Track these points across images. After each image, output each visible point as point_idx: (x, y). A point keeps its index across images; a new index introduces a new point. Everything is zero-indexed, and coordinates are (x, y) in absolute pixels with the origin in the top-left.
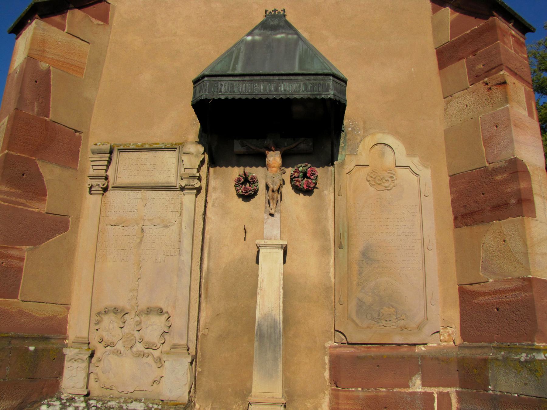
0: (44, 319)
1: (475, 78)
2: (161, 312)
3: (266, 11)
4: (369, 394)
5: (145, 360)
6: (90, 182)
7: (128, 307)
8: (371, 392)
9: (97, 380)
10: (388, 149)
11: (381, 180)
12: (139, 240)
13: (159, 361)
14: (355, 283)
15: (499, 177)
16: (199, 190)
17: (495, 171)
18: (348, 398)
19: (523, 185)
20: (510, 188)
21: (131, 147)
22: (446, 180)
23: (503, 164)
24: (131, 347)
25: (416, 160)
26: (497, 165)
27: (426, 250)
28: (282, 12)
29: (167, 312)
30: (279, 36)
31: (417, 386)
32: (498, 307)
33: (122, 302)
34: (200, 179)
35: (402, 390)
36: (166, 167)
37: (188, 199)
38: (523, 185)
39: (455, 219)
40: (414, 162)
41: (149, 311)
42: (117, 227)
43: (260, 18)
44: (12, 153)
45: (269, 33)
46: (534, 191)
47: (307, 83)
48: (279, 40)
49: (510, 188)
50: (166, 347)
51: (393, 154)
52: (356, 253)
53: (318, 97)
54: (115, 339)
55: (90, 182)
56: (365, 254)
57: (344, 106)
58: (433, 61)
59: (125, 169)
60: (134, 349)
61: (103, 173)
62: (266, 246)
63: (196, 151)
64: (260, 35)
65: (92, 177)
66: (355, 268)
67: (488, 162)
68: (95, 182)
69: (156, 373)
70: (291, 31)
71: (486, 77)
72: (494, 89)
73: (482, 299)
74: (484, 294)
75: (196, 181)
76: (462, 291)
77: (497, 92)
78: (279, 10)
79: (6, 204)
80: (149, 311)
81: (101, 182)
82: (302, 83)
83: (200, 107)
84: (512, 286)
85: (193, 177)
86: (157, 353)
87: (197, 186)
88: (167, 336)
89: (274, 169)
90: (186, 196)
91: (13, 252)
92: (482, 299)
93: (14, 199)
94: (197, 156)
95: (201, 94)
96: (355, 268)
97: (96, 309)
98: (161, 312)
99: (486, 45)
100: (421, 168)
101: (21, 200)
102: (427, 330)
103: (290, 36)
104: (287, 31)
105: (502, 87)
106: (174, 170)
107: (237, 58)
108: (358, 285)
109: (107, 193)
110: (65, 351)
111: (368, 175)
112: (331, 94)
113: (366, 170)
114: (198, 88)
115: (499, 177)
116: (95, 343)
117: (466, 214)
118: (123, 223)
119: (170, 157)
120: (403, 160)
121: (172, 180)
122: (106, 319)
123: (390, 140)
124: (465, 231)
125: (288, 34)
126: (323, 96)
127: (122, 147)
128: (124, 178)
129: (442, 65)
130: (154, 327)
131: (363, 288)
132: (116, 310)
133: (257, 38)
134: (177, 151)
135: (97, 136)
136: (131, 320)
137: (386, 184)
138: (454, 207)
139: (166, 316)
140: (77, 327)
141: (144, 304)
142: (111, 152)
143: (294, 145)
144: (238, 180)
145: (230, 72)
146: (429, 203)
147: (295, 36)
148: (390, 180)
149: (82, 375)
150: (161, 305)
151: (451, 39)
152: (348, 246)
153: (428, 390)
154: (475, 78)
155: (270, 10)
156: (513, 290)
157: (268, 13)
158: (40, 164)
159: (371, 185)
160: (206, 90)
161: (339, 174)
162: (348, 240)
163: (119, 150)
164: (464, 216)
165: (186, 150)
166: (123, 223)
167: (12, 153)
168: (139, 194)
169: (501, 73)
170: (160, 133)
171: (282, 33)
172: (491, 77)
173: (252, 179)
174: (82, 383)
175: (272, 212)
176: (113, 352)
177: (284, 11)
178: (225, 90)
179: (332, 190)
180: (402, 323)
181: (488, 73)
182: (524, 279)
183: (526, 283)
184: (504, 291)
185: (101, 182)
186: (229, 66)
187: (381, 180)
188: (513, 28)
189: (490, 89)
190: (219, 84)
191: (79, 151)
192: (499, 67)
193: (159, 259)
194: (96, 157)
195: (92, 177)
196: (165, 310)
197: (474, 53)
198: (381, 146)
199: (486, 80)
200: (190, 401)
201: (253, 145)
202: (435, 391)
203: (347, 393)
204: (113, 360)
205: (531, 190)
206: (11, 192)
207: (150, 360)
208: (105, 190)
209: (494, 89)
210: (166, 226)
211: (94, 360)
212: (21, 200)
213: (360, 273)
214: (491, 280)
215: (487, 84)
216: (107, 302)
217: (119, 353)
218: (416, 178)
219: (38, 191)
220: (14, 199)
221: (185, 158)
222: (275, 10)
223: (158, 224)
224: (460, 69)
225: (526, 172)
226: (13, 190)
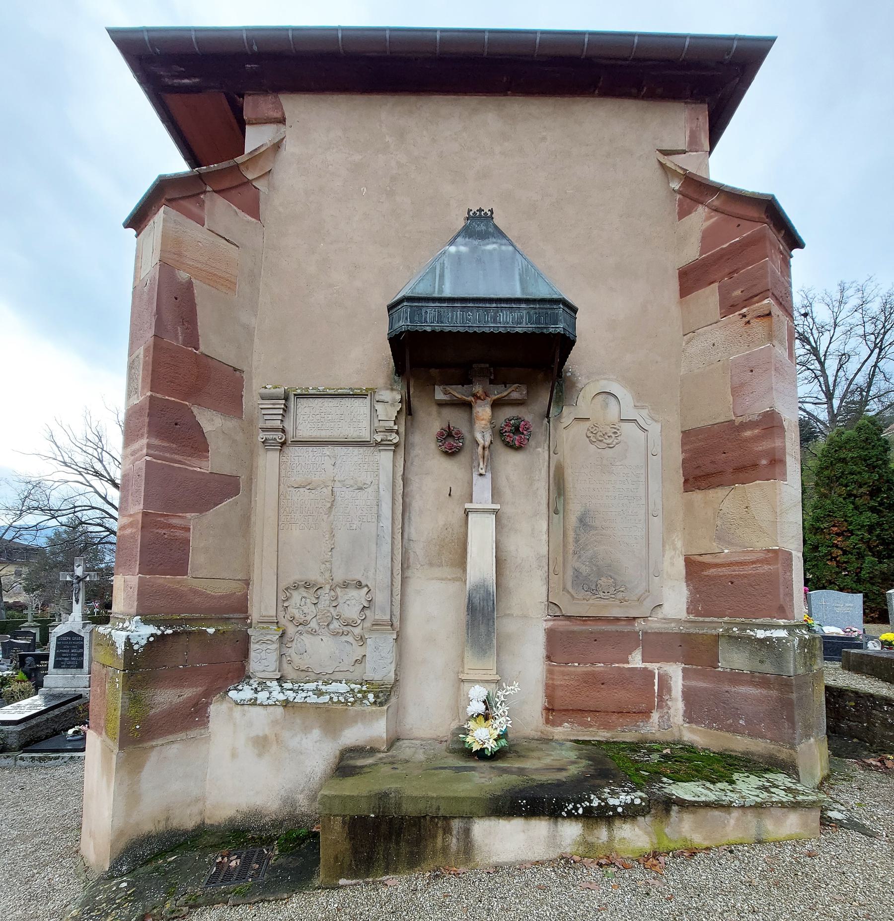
0: (221, 597)
1: (729, 307)
2: (359, 585)
3: (470, 211)
4: (585, 670)
5: (344, 638)
6: (262, 436)
7: (321, 580)
8: (588, 668)
9: (290, 662)
10: (612, 399)
11: (602, 437)
12: (329, 505)
13: (362, 639)
14: (571, 551)
15: (748, 433)
16: (396, 445)
17: (744, 426)
18: (563, 674)
19: (778, 443)
20: (765, 445)
21: (311, 392)
22: (678, 436)
23: (755, 418)
24: (328, 625)
25: (644, 413)
26: (745, 419)
27: (651, 517)
28: (489, 213)
29: (367, 586)
30: (490, 247)
31: (636, 661)
32: (733, 580)
33: (313, 576)
34: (397, 433)
35: (621, 665)
36: (355, 419)
37: (385, 458)
38: (778, 443)
39: (686, 481)
40: (642, 416)
41: (345, 585)
42: (302, 490)
43: (461, 223)
44: (159, 396)
45: (476, 242)
46: (787, 451)
47: (532, 312)
48: (491, 252)
49: (765, 445)
50: (367, 624)
51: (618, 406)
52: (573, 520)
53: (545, 331)
54: (309, 618)
55: (262, 436)
56: (582, 521)
57: (572, 343)
58: (674, 285)
59: (308, 419)
60: (331, 627)
61: (277, 424)
62: (476, 511)
63: (390, 399)
64: (465, 245)
65: (264, 430)
66: (571, 535)
67: (735, 414)
68: (270, 435)
69: (358, 653)
70: (504, 241)
71: (745, 307)
72: (754, 322)
73: (712, 571)
74: (716, 565)
75: (394, 435)
76: (690, 563)
77: (758, 327)
78: (486, 210)
79: (159, 461)
80: (345, 585)
81: (278, 436)
82: (525, 312)
83: (391, 340)
84: (753, 557)
85: (390, 431)
86: (357, 631)
87: (395, 441)
88: (367, 612)
89: (483, 422)
90: (382, 453)
91: (174, 521)
92: (712, 571)
93: (168, 455)
94: (393, 405)
95: (401, 323)
96: (571, 535)
97: (283, 585)
98: (359, 585)
99: (748, 264)
100: (649, 421)
101: (177, 457)
102: (648, 604)
103: (503, 248)
104: (499, 241)
105: (766, 320)
106: (366, 423)
107: (442, 276)
108: (575, 553)
109: (285, 448)
110: (250, 631)
111: (588, 430)
112: (560, 327)
113: (587, 424)
114: (395, 316)
115: (748, 433)
116: (283, 622)
117: (700, 477)
118: (309, 486)
119: (361, 407)
120: (629, 411)
121: (366, 435)
122: (296, 596)
123: (615, 388)
124: (697, 496)
125: (501, 244)
126: (551, 330)
127: (299, 391)
128: (305, 431)
129: (684, 291)
130: (351, 604)
131: (580, 557)
132: (307, 586)
133: (463, 249)
134: (368, 398)
135: (262, 379)
136: (325, 596)
137: (609, 441)
138: (684, 469)
139: (366, 589)
140: (262, 604)
141: (339, 577)
142: (286, 398)
143: (505, 393)
144: (441, 434)
145: (436, 295)
146: (655, 463)
147: (511, 248)
148: (613, 436)
149: (273, 657)
150: (359, 577)
151: (700, 255)
152: (564, 511)
153: (649, 666)
154: (729, 307)
155: (474, 210)
156: (753, 563)
157: (471, 213)
158: (195, 410)
159: (592, 442)
160: (406, 319)
161: (555, 429)
162: (564, 505)
163: (295, 395)
164: (696, 478)
165: (377, 398)
166: (309, 486)
167: (159, 396)
168: (327, 450)
169: (766, 301)
170: (348, 376)
171: (494, 243)
172: (752, 307)
173: (457, 434)
174: (273, 665)
175: (483, 472)
176: (308, 632)
177: (491, 211)
178: (430, 321)
179: (546, 448)
180: (620, 595)
181: (748, 301)
182: (769, 551)
183: (770, 555)
184: (741, 563)
185: (278, 436)
186: (434, 287)
187: (602, 437)
188: (782, 241)
189: (748, 322)
190: (423, 312)
191: (242, 396)
192: (763, 294)
193: (354, 527)
194: (267, 404)
195: (264, 430)
196: (364, 583)
197: (730, 274)
198: (604, 396)
199: (744, 310)
200: (396, 681)
201: (458, 392)
202: (654, 667)
203: (562, 669)
204: (307, 639)
205: (784, 449)
206: (164, 447)
207: (350, 639)
208: (283, 444)
209: (754, 322)
210: (360, 489)
211: (285, 639)
212: (177, 457)
213: (577, 541)
214: (726, 551)
215: (744, 316)
216: (296, 576)
217: (313, 633)
218: (642, 434)
219: (197, 444)
220: (168, 455)
221: (379, 407)
222: (480, 210)
223: (351, 486)
224: (709, 297)
225: (782, 427)
226: (166, 444)
